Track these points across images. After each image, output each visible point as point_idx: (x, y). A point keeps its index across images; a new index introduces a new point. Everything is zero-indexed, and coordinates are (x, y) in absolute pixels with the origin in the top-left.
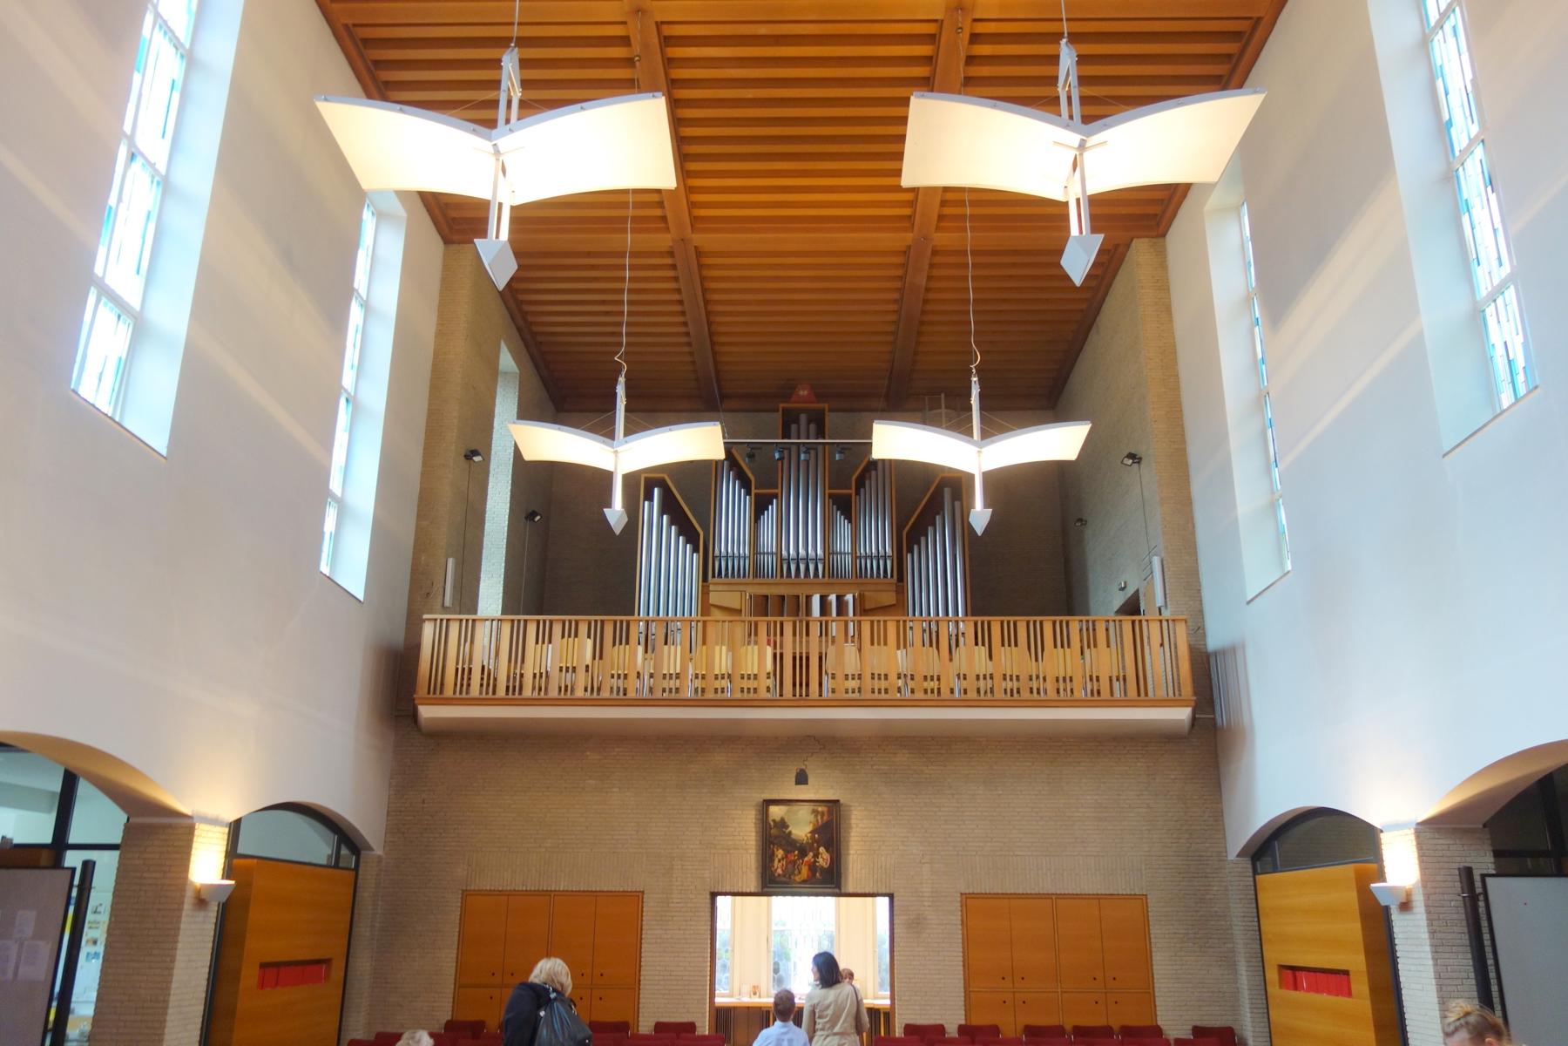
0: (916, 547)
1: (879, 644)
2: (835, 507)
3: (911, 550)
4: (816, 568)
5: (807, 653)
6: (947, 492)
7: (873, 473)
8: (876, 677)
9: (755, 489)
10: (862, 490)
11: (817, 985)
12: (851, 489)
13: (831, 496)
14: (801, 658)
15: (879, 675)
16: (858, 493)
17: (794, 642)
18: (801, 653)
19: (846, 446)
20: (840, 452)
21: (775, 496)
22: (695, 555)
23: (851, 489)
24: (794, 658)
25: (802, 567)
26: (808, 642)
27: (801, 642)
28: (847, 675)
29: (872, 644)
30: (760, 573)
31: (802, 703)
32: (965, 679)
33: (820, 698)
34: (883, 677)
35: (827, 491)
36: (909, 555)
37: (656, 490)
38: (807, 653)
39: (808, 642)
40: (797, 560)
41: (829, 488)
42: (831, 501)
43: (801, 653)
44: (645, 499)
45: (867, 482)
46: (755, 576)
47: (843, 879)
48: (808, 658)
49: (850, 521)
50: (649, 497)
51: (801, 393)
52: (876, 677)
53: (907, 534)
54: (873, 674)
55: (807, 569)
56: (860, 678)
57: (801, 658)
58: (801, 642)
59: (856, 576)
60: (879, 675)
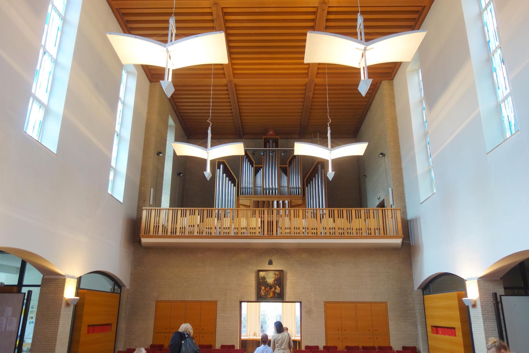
0: (309, 185)
1: (297, 217)
2: (282, 171)
3: (307, 186)
4: (275, 192)
5: (272, 220)
6: (320, 166)
7: (295, 160)
8: (296, 228)
9: (255, 165)
10: (291, 165)
12: (287, 165)
13: (280, 167)
14: (270, 222)
15: (297, 228)
16: (289, 166)
17: (268, 217)
18: (270, 220)
19: (285, 151)
20: (283, 153)
21: (262, 167)
22: (234, 187)
23: (287, 165)
24: (268, 222)
25: (271, 191)
26: (272, 217)
27: (270, 217)
28: (286, 228)
29: (294, 217)
30: (256, 193)
31: (270, 237)
32: (325, 229)
33: (277, 236)
34: (298, 228)
35: (279, 166)
36: (307, 187)
37: (221, 165)
38: (272, 220)
39: (272, 217)
40: (269, 189)
41: (280, 165)
42: (280, 169)
43: (270, 220)
44: (218, 169)
45: (293, 163)
46: (255, 194)
47: (284, 297)
48: (272, 222)
49: (287, 176)
50: (219, 168)
51: (270, 133)
52: (296, 228)
53: (306, 180)
54: (294, 228)
55: (272, 192)
56: (290, 229)
57: (270, 222)
58: (270, 217)
59: (289, 195)
60: (297, 228)
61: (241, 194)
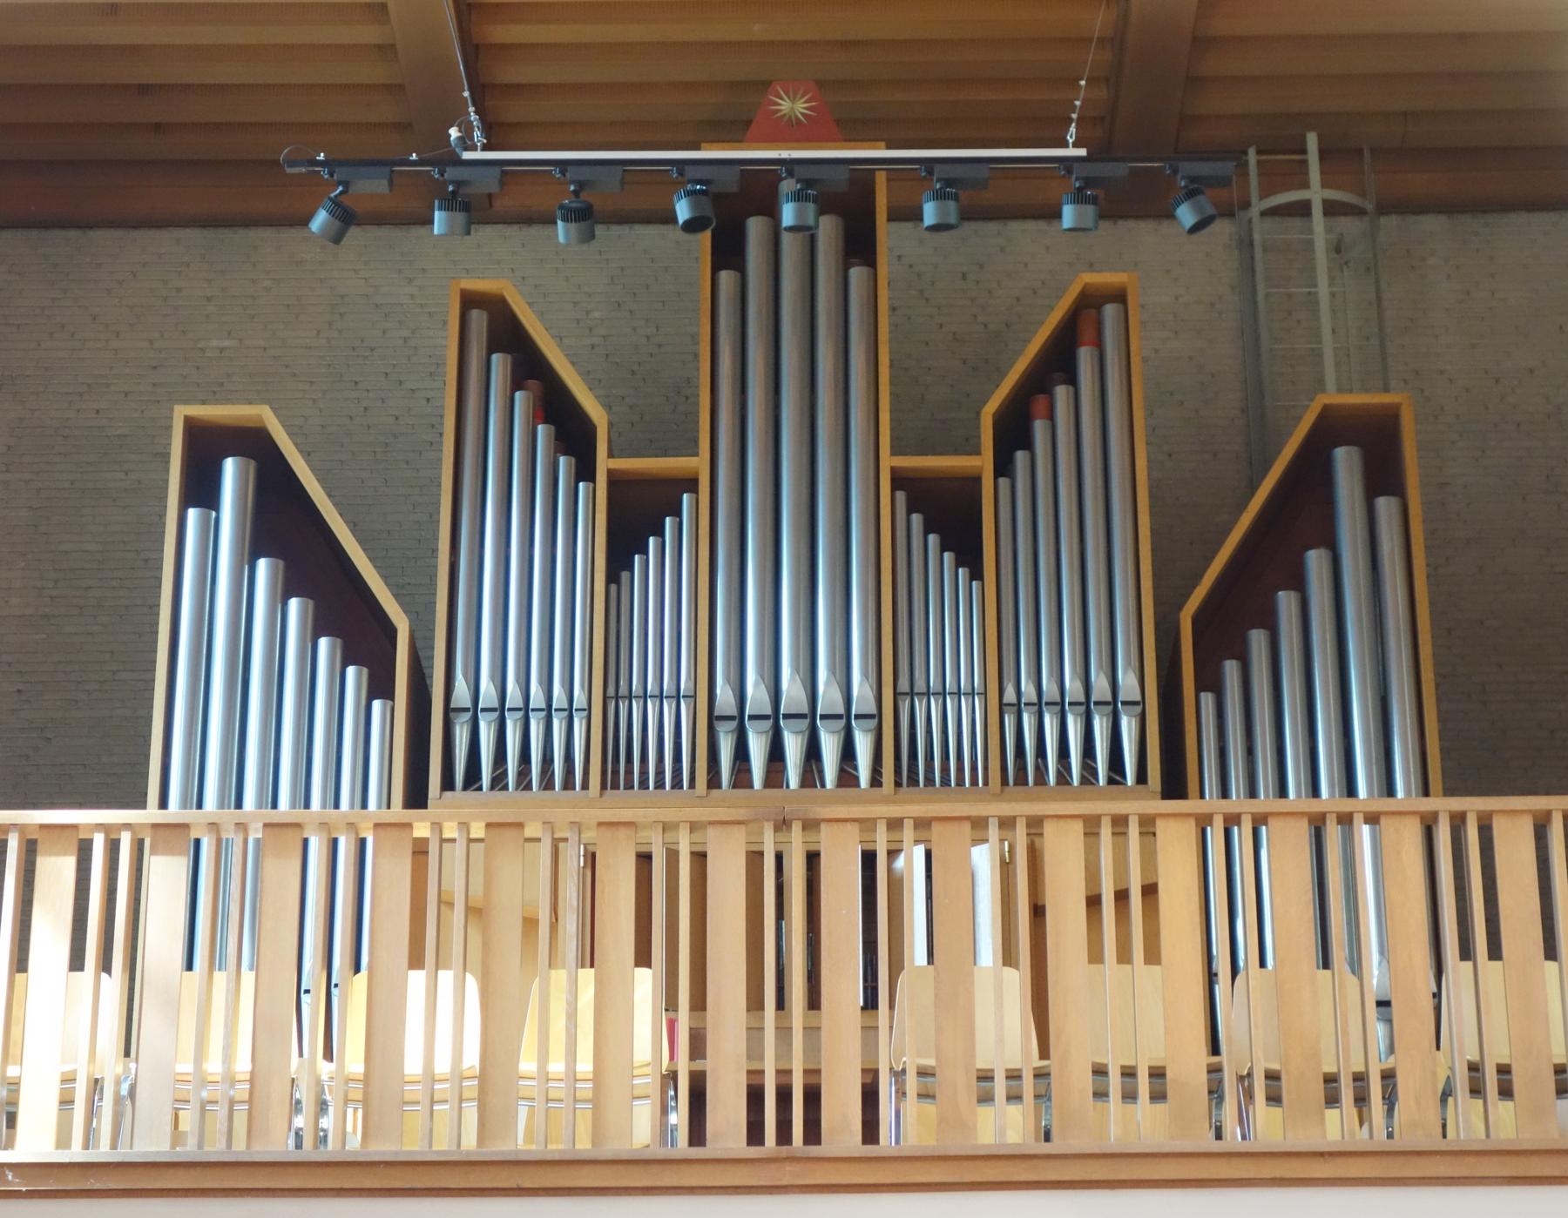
0: (1231, 668)
1: (1124, 956)
2: (916, 518)
3: (1210, 681)
4: (848, 753)
5: (812, 1073)
6: (1346, 463)
7: (1062, 393)
8: (1115, 1081)
9: (611, 455)
10: (1021, 457)
11: (1115, 223)
12: (976, 451)
13: (900, 480)
14: (784, 1096)
15: (1129, 1073)
16: (1003, 467)
17: (755, 1032)
18: (784, 1074)
19: (957, 172)
20: (940, 196)
21: (691, 484)
22: (377, 705)
23: (976, 451)
24: (755, 1097)
25: (793, 747)
26: (812, 1031)
27: (784, 1032)
28: (986, 1077)
29: (1096, 956)
30: (629, 772)
31: (787, 1174)
32: (1506, 1092)
33: (870, 1150)
34: (1143, 1084)
35: (888, 461)
36: (1207, 699)
37: (230, 466)
38: (812, 1073)
39: (812, 1031)
40: (775, 719)
41: (895, 451)
42: (901, 496)
43: (784, 1074)
44: (187, 501)
45: (1039, 428)
46: (610, 781)
47: (357, 896)
48: (813, 1097)
49: (977, 574)
50: (201, 491)
51: (785, 106)
52: (1115, 1081)
53: (1196, 620)
54: (1100, 1071)
55: (813, 753)
56: (1042, 1097)
57: (784, 1096)
58: (784, 1032)
59: (1005, 782)
60: (1129, 1073)
61: (448, 784)
